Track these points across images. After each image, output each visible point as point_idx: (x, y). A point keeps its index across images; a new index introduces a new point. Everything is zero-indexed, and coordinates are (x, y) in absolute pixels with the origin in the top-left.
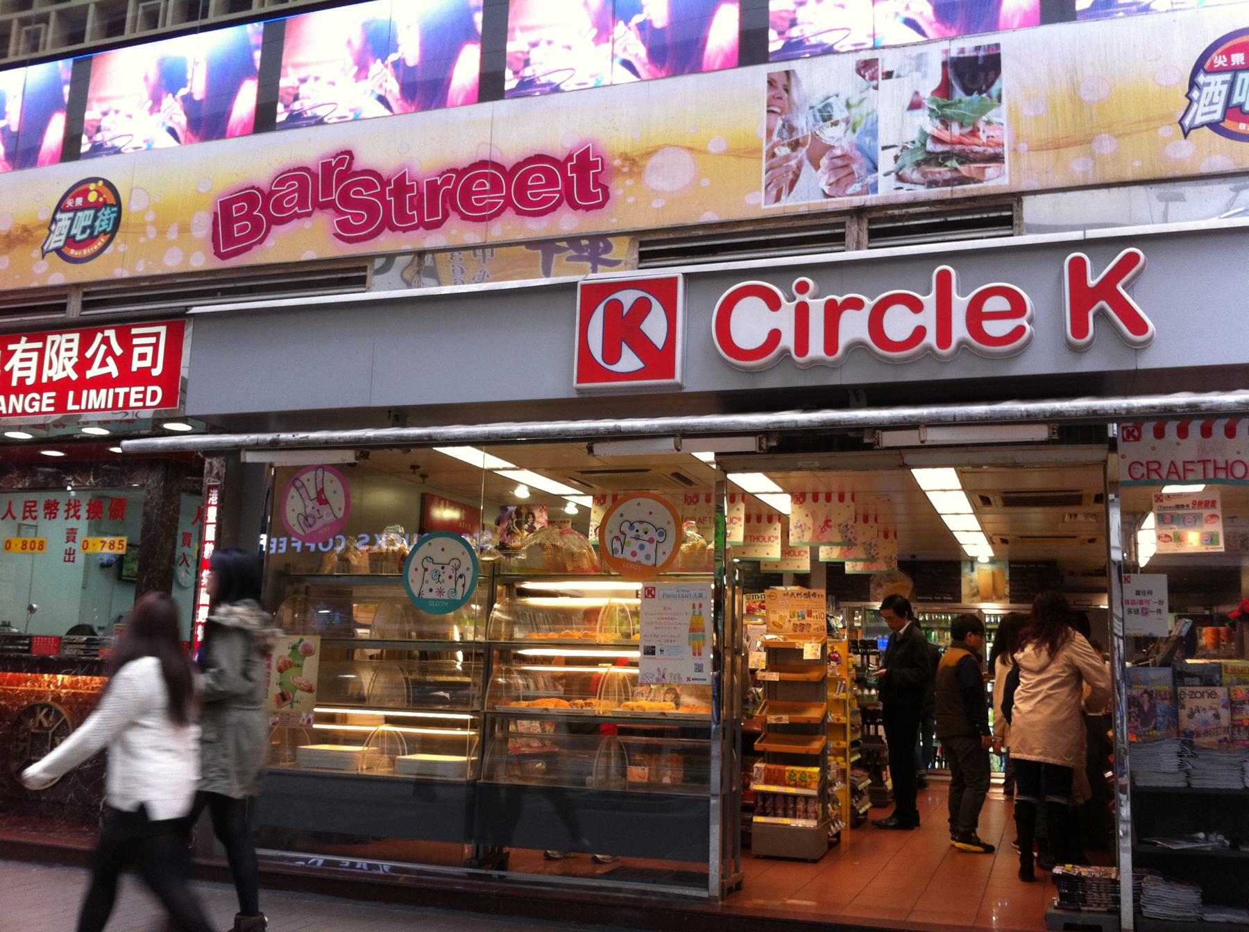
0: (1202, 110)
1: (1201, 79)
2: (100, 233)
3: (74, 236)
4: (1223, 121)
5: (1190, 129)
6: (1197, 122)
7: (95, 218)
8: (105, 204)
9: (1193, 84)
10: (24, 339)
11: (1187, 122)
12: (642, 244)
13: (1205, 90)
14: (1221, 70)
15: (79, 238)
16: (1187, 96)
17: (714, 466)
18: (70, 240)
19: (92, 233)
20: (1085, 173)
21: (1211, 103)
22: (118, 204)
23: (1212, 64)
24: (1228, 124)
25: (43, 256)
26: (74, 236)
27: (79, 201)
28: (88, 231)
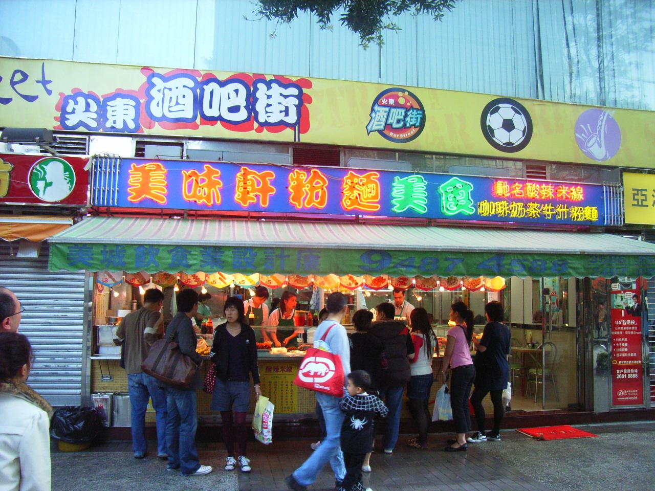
0: (376, 123)
1: (376, 108)
2: (411, 126)
3: (391, 124)
4: (384, 130)
5: (370, 132)
6: (373, 129)
7: (406, 116)
8: (412, 107)
9: (372, 110)
10: (583, 199)
11: (369, 128)
12: (527, 167)
13: (378, 113)
14: (385, 106)
15: (395, 126)
16: (370, 115)
17: (438, 282)
18: (388, 126)
19: (405, 125)
20: (605, 158)
21: (380, 121)
22: (422, 108)
23: (381, 102)
24: (386, 132)
25: (368, 134)
26: (391, 124)
27: (392, 102)
28: (402, 123)
